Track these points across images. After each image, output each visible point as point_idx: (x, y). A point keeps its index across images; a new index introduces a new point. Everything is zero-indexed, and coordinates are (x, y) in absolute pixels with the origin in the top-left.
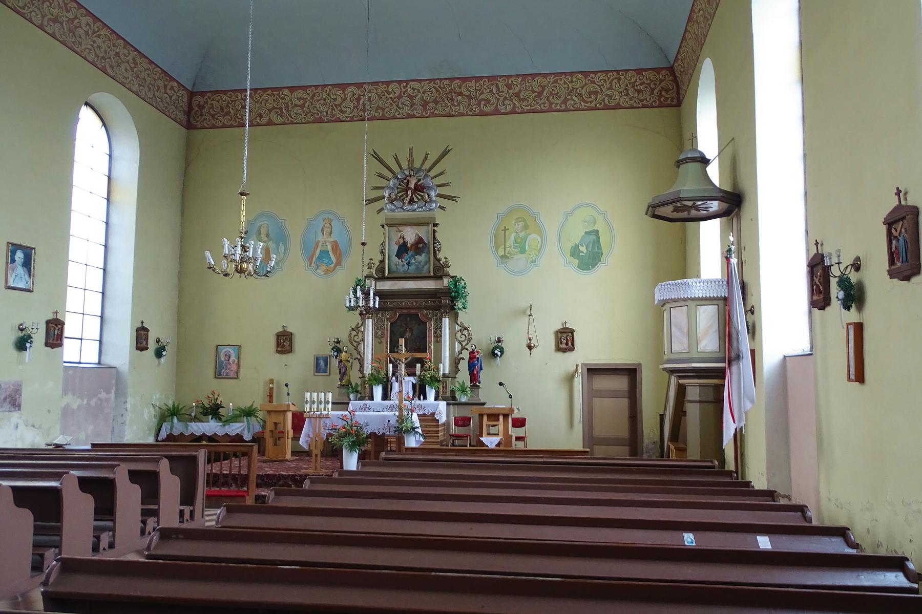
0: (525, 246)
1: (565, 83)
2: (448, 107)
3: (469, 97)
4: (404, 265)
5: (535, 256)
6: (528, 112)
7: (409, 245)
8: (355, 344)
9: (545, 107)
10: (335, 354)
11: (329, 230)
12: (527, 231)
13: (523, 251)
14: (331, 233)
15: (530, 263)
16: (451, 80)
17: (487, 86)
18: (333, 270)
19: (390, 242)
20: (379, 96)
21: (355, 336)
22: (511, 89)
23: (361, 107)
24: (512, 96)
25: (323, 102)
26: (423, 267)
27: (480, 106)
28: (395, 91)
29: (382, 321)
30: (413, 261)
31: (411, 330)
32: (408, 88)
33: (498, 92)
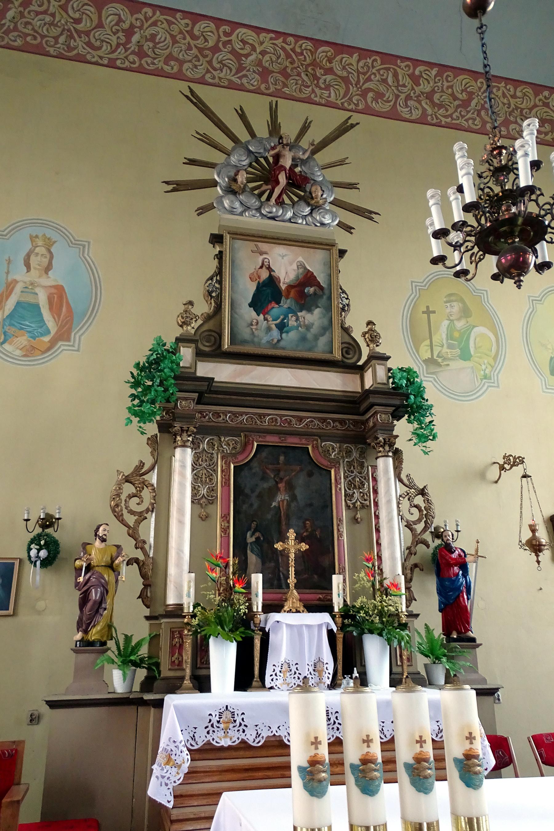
0: (469, 344)
1: (504, 95)
2: (308, 87)
3: (346, 80)
4: (269, 329)
5: (489, 367)
6: (447, 126)
7: (283, 287)
8: (131, 520)
9: (476, 125)
10: (43, 554)
11: (46, 261)
12: (469, 319)
13: (465, 355)
14: (48, 268)
15: (482, 380)
16: (318, 43)
17: (378, 70)
18: (49, 349)
19: (236, 272)
20: (173, 37)
21: (130, 497)
22: (418, 84)
23: (132, 46)
24: (419, 96)
25: (48, 19)
26: (316, 338)
27: (365, 100)
28: (207, 37)
29: (211, 459)
30: (292, 322)
31: (290, 487)
32: (233, 37)
33: (396, 84)
